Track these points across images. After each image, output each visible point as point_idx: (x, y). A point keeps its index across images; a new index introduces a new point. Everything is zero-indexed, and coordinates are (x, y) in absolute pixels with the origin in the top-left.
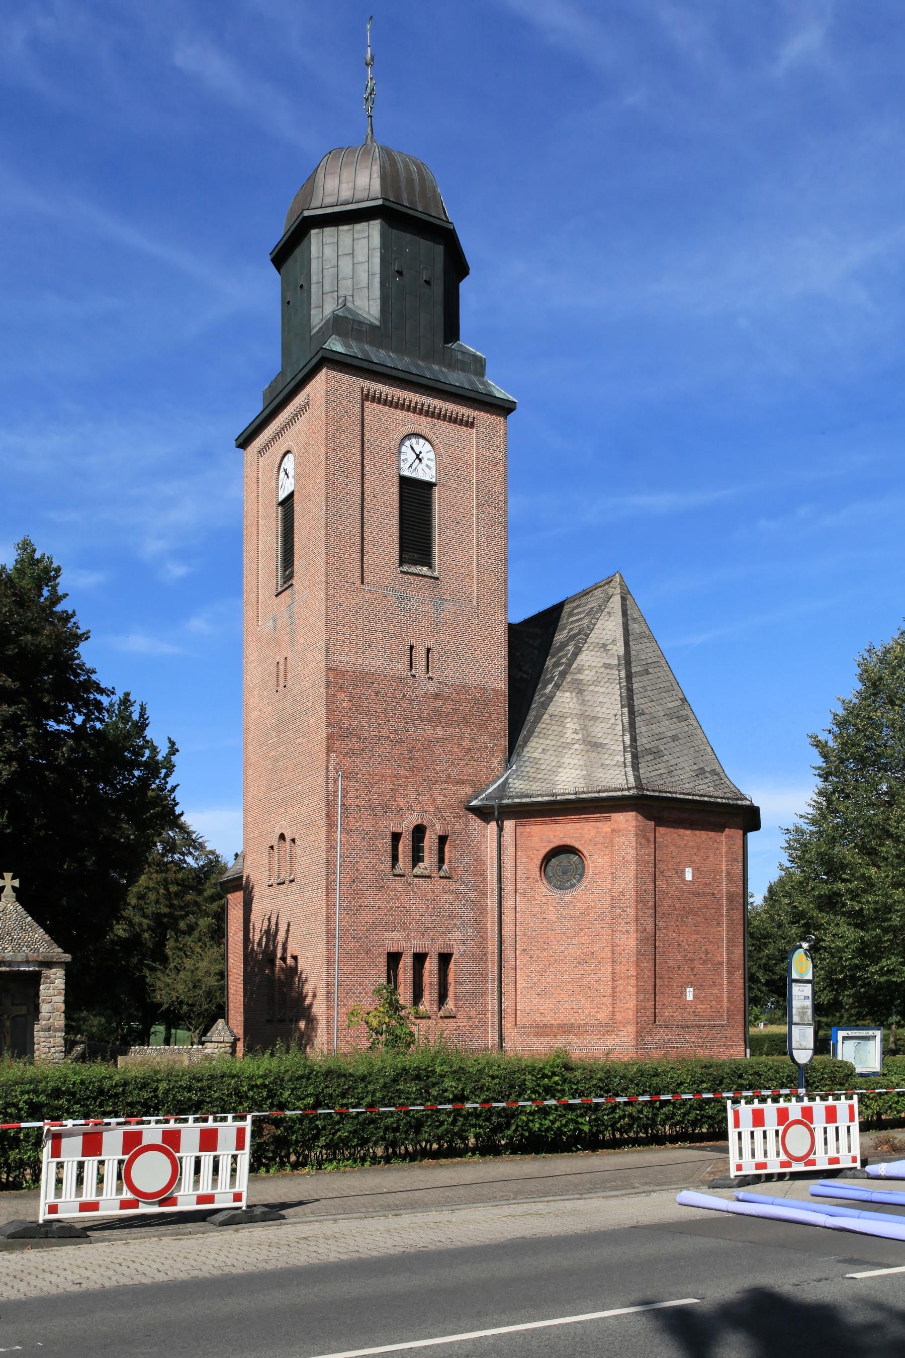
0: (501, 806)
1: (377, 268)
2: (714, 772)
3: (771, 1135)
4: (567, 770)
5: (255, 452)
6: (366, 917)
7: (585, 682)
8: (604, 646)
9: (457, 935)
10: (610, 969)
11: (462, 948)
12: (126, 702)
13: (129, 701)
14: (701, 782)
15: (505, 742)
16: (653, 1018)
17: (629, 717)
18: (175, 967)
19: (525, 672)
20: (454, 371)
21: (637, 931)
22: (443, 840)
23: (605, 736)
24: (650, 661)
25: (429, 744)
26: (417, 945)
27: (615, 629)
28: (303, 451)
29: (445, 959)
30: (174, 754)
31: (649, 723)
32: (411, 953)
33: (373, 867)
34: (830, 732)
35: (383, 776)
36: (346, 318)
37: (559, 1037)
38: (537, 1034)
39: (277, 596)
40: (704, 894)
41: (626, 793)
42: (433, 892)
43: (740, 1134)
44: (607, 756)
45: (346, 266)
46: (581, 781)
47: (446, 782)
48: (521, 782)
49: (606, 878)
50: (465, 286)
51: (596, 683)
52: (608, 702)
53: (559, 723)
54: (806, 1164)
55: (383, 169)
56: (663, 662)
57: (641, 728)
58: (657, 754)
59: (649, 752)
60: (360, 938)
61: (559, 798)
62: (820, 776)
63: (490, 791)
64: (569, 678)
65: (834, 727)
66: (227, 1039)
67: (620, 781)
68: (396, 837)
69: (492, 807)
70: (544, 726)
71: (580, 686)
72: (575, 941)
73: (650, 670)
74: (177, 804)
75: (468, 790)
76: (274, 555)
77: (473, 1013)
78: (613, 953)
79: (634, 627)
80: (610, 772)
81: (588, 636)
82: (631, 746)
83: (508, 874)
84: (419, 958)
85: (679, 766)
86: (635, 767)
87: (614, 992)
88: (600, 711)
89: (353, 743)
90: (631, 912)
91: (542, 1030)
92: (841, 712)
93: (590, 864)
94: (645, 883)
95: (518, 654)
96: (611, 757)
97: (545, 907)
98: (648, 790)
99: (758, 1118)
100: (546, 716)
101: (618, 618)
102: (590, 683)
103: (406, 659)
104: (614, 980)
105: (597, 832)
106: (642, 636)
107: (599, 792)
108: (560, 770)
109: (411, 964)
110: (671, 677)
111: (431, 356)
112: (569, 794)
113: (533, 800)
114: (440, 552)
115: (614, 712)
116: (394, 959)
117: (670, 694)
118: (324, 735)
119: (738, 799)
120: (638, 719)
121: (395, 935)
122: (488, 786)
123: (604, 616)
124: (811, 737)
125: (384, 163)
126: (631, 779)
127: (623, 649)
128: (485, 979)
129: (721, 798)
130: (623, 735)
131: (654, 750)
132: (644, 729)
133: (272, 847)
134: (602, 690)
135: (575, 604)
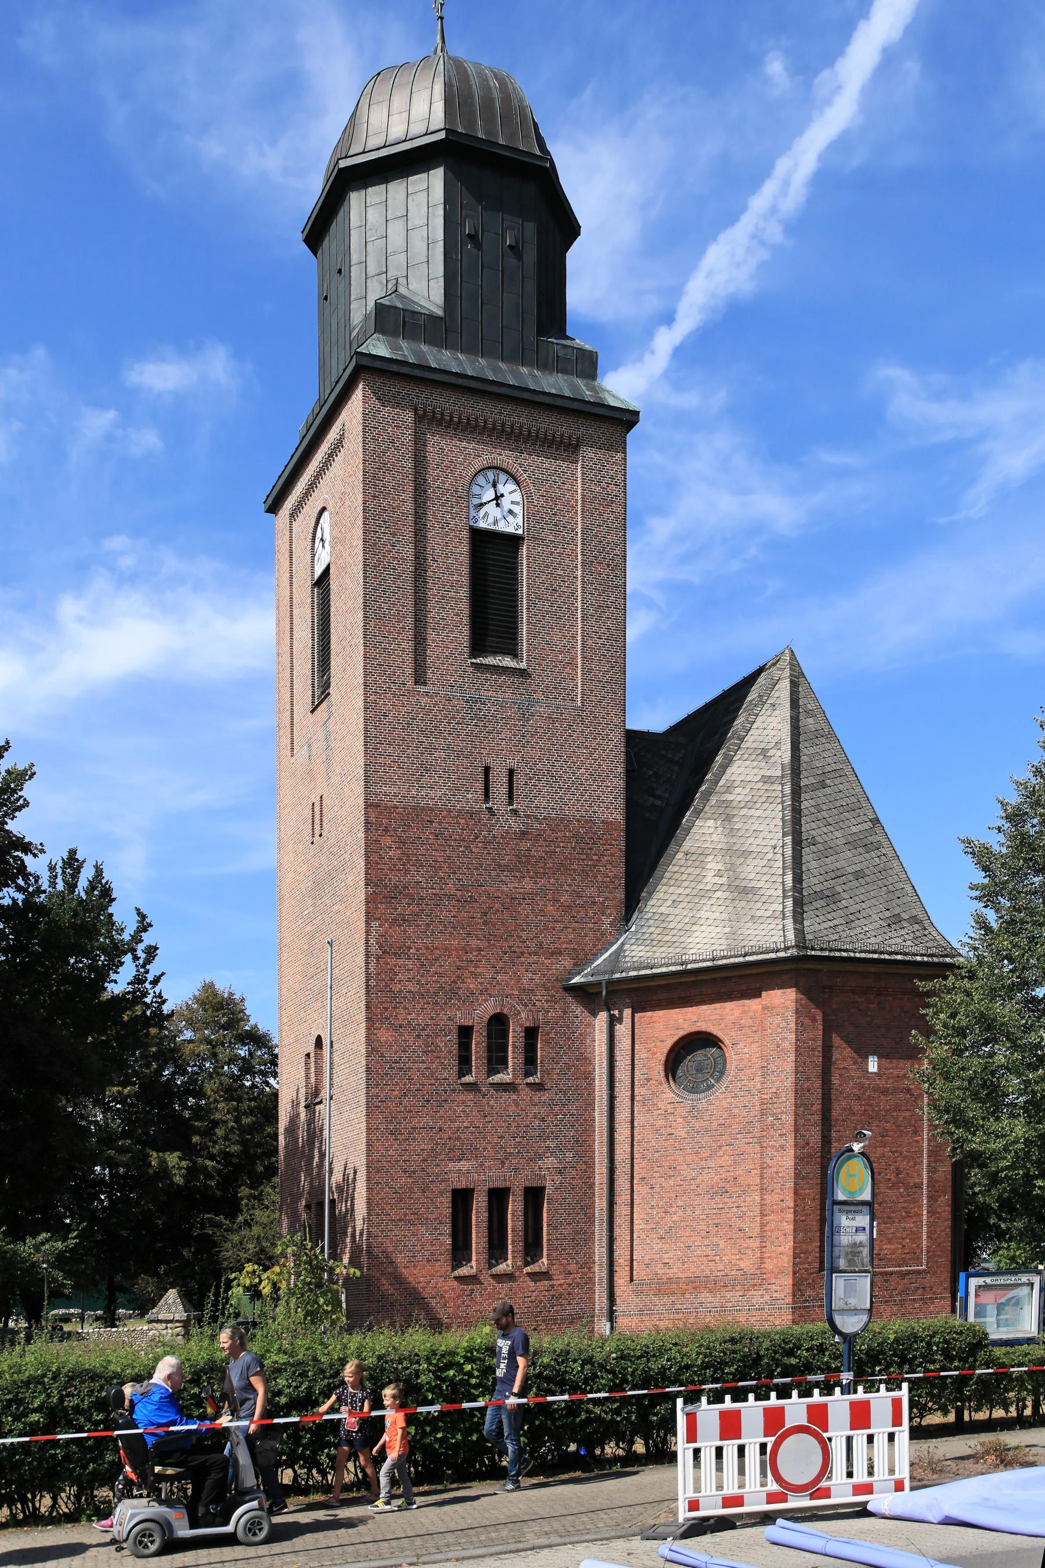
0: (610, 983)
1: (440, 234)
2: (915, 920)
3: (753, 1455)
4: (703, 928)
5: (288, 516)
6: (422, 1144)
7: (735, 804)
8: (764, 752)
9: (550, 1161)
10: (758, 1199)
11: (558, 1179)
12: (73, 863)
13: (77, 860)
14: (894, 934)
15: (620, 894)
16: (817, 1265)
17: (793, 849)
18: (246, 1221)
19: (659, 798)
20: (551, 373)
21: (796, 1145)
22: (531, 1034)
23: (759, 877)
24: (828, 769)
25: (512, 901)
26: (493, 1176)
27: (779, 726)
28: (339, 504)
29: (534, 1196)
30: (145, 930)
31: (821, 856)
32: (486, 1188)
33: (432, 1074)
34: (999, 829)
35: (446, 949)
36: (395, 307)
37: (687, 1296)
38: (658, 1293)
39: (312, 712)
40: (895, 1090)
41: (782, 954)
42: (517, 1105)
43: (697, 1452)
44: (759, 905)
45: (396, 238)
46: (722, 941)
47: (536, 953)
48: (641, 948)
49: (755, 1074)
50: (575, 256)
51: (750, 804)
52: (766, 829)
53: (697, 863)
54: (812, 1497)
55: (448, 86)
56: (847, 770)
57: (810, 862)
58: (831, 898)
59: (819, 895)
60: (414, 1172)
61: (689, 967)
62: (978, 899)
63: (598, 962)
64: (713, 800)
65: (1004, 822)
66: (177, 1317)
67: (775, 939)
68: (465, 1032)
69: (599, 984)
70: (676, 869)
71: (728, 811)
72: (711, 1164)
73: (828, 782)
74: (164, 1002)
75: (567, 963)
76: (310, 656)
77: (573, 1267)
78: (762, 1177)
79: (808, 723)
80: (763, 926)
81: (742, 739)
82: (794, 888)
83: (622, 1075)
84: (498, 1197)
85: (864, 913)
86: (798, 916)
87: (762, 1231)
88: (753, 844)
89: (404, 908)
90: (789, 1119)
91: (664, 1287)
92: (1014, 799)
93: (730, 1053)
94: (808, 1079)
95: (651, 773)
96: (766, 906)
97: (671, 1118)
98: (813, 949)
99: (730, 1426)
100: (679, 855)
101: (785, 711)
102: (742, 804)
103: (479, 786)
104: (763, 1215)
105: (744, 1012)
106: (818, 734)
107: (745, 955)
108: (695, 928)
109: (485, 1204)
110: (858, 790)
111: (519, 356)
112: (704, 960)
113: (655, 971)
114: (529, 632)
115: (773, 843)
116: (462, 1198)
117: (855, 814)
118: (363, 897)
119: (946, 956)
120: (806, 851)
121: (464, 1165)
122: (596, 956)
123: (766, 710)
124: (963, 841)
125: (450, 78)
126: (791, 935)
127: (789, 754)
128: (591, 1220)
129: (922, 955)
130: (783, 875)
131: (827, 893)
132: (814, 864)
133: (308, 1055)
134: (758, 813)
135: (732, 699)
